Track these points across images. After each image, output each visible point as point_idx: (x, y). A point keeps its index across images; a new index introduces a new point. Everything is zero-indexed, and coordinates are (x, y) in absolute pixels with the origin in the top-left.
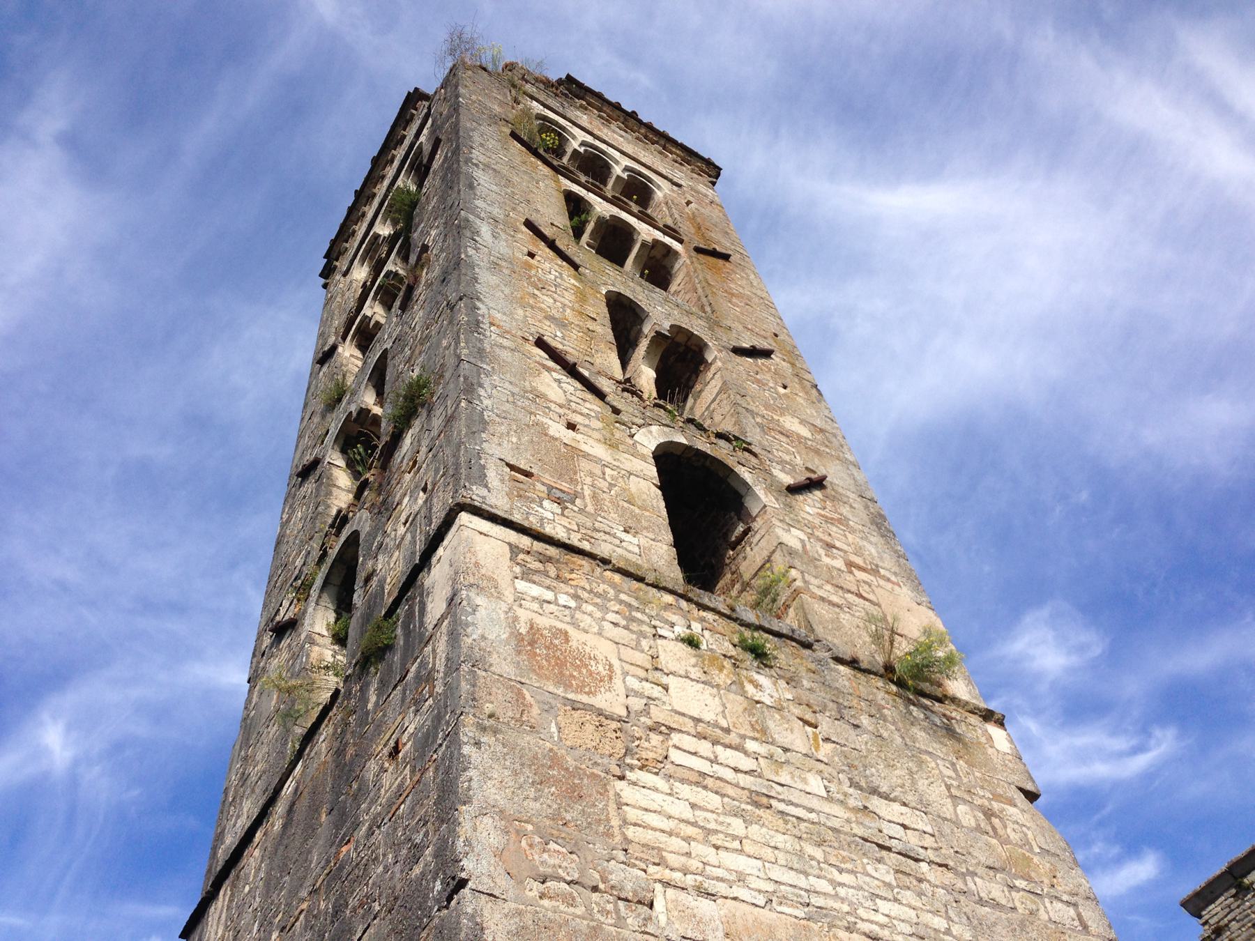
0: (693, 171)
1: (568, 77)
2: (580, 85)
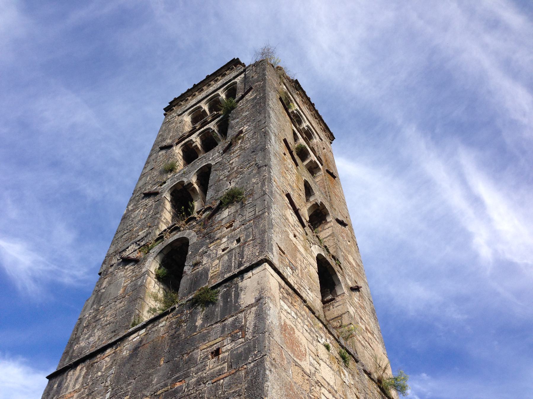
0: (326, 135)
1: (297, 80)
2: (299, 86)
